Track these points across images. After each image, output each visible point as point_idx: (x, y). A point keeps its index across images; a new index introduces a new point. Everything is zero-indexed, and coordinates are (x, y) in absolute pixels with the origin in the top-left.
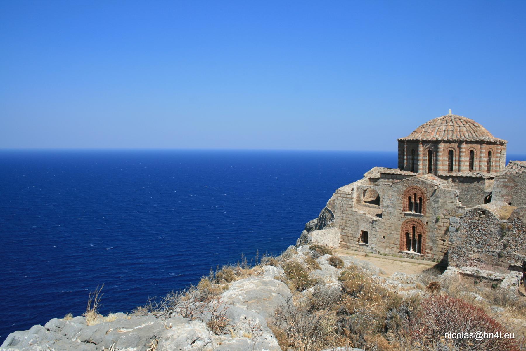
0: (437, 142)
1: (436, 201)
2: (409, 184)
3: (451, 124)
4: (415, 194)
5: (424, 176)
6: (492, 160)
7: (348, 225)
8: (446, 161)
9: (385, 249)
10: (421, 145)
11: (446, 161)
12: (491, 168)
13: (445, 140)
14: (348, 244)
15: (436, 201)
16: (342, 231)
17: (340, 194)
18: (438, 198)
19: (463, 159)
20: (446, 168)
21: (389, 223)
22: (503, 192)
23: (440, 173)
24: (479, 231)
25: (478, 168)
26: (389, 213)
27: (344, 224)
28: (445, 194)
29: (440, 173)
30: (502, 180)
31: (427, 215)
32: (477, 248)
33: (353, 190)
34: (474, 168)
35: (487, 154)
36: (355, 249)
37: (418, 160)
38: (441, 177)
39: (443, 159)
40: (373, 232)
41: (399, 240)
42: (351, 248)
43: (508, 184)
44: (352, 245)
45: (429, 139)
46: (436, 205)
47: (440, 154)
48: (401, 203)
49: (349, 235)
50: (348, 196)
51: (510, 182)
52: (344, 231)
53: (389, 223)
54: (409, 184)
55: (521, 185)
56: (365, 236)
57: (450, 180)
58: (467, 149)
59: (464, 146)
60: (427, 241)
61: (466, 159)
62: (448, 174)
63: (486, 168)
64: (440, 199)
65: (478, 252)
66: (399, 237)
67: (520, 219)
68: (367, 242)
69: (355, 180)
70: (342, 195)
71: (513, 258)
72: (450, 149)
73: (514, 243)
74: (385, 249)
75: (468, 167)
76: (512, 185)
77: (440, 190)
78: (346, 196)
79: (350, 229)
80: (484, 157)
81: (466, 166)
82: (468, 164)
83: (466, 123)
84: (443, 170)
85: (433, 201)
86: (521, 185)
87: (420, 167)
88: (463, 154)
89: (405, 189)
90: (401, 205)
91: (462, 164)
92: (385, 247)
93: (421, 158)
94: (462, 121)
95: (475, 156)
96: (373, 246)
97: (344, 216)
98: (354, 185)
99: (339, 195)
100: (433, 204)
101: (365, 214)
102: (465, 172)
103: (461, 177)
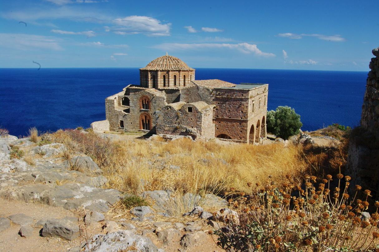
0: (168, 72)
1: (155, 103)
2: (142, 94)
3: (165, 61)
4: (145, 99)
5: (151, 90)
6: (186, 80)
7: (113, 118)
8: (162, 81)
9: (132, 129)
10: (149, 73)
11: (162, 81)
12: (186, 84)
13: (161, 70)
14: (114, 128)
15: (155, 103)
16: (110, 121)
17: (108, 101)
18: (156, 101)
19: (170, 80)
20: (163, 85)
21: (133, 116)
22: (185, 97)
23: (159, 87)
24: (169, 117)
25: (178, 85)
26: (133, 110)
27: (111, 118)
28: (159, 99)
29: (159, 87)
30: (184, 91)
31: (152, 110)
32: (168, 125)
33: (115, 98)
34: (177, 84)
35: (183, 77)
36: (118, 130)
37: (157, 81)
38: (160, 90)
39: (160, 81)
40: (126, 121)
41: (139, 124)
42: (116, 130)
43: (187, 93)
44: (116, 129)
45: (153, 70)
46: (155, 105)
47: (159, 77)
48: (139, 104)
49: (114, 123)
50: (112, 102)
51: (188, 92)
52: (111, 121)
53: (133, 116)
54: (142, 94)
55: (192, 93)
56: (122, 123)
57: (164, 91)
58: (172, 75)
59: (181, 73)
60: (152, 123)
61: (182, 80)
62: (163, 88)
63: (183, 84)
64: (157, 102)
65: (169, 126)
66: (138, 122)
67: (184, 110)
68: (123, 127)
69: (117, 93)
70: (109, 102)
71: (182, 128)
72: (164, 75)
73: (183, 121)
74: (132, 129)
75: (173, 84)
76: (188, 93)
77: (157, 97)
78: (110, 102)
79: (114, 120)
80: (182, 78)
81: (172, 83)
82: (173, 82)
83: (174, 60)
84: (161, 86)
85: (154, 102)
86: (192, 93)
87: (150, 85)
88: (170, 77)
89: (140, 97)
90: (139, 105)
91: (170, 82)
92: (132, 128)
93: (159, 80)
94: (172, 59)
95: (176, 78)
96: (127, 128)
97: (111, 113)
98: (116, 96)
99: (107, 102)
100: (154, 104)
101: (121, 111)
102: (172, 86)
103: (169, 89)
